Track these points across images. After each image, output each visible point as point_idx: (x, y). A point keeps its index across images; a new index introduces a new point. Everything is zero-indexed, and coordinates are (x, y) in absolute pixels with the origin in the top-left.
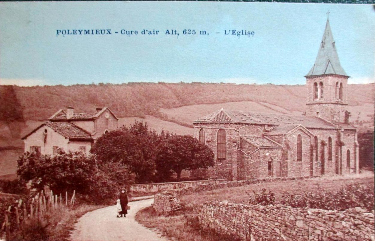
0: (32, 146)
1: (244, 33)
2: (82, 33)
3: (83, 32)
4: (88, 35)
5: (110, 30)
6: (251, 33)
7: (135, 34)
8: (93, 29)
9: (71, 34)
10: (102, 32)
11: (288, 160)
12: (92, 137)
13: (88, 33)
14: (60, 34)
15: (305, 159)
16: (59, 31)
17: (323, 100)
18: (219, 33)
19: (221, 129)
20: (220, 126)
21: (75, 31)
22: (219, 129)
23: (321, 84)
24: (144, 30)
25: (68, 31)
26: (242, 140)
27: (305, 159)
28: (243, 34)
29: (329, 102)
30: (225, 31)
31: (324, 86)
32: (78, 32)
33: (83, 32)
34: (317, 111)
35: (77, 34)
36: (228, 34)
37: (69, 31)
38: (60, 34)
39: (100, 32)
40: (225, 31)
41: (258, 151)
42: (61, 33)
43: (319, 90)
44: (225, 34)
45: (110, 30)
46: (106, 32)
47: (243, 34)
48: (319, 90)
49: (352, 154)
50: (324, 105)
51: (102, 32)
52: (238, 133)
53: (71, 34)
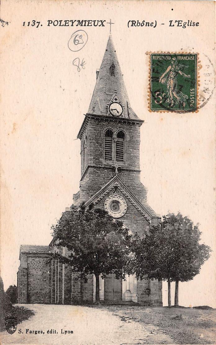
1: (189, 24)
3: (76, 23)
9: (63, 25)
14: (51, 25)
47: (188, 25)
53: (63, 25)
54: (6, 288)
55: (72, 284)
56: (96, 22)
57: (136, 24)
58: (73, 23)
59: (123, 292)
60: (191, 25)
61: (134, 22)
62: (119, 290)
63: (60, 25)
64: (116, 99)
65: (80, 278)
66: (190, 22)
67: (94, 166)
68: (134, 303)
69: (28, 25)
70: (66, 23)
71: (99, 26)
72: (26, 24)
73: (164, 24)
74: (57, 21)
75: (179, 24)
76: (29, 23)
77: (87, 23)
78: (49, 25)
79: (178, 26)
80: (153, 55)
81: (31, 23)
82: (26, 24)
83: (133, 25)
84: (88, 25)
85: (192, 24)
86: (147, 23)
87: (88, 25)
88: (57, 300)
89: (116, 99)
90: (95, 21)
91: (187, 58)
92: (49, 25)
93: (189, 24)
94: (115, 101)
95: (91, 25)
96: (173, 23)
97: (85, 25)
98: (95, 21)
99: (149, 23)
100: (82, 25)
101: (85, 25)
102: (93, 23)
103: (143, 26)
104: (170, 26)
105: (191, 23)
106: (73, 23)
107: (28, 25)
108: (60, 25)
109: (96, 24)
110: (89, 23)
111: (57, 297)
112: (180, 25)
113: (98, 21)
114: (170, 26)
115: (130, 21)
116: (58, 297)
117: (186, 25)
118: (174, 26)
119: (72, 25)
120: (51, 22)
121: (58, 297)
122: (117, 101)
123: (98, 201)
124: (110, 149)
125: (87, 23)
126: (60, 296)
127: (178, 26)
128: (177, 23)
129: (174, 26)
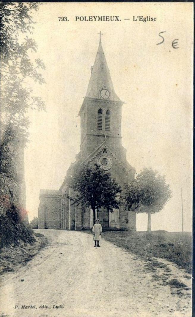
0: (40, 85)
2: (96, 20)
3: (97, 19)
4: (100, 21)
5: (118, 17)
6: (153, 19)
8: (134, 16)
9: (88, 20)
10: (111, 19)
12: (178, 296)
13: (101, 20)
14: (78, 20)
16: (77, 18)
24: (147, 17)
25: (85, 17)
30: (134, 17)
32: (93, 19)
33: (88, 18)
35: (92, 20)
36: (136, 20)
37: (86, 18)
38: (78, 20)
39: (110, 18)
40: (134, 17)
42: (79, 19)
44: (134, 20)
45: (118, 17)
46: (115, 18)
47: (147, 20)
49: (191, 303)
51: (111, 19)
53: (88, 20)
55: (76, 216)
59: (110, 222)
60: (149, 20)
62: (107, 220)
64: (105, 87)
66: (149, 17)
67: (90, 134)
68: (118, 229)
70: (90, 18)
73: (129, 19)
74: (112, 20)
85: (151, 19)
87: (106, 20)
88: (65, 227)
89: (105, 87)
94: (104, 88)
105: (150, 18)
109: (112, 19)
111: (65, 225)
116: (66, 225)
121: (66, 225)
122: (106, 88)
123: (93, 158)
124: (101, 121)
126: (67, 224)
129: (136, 20)
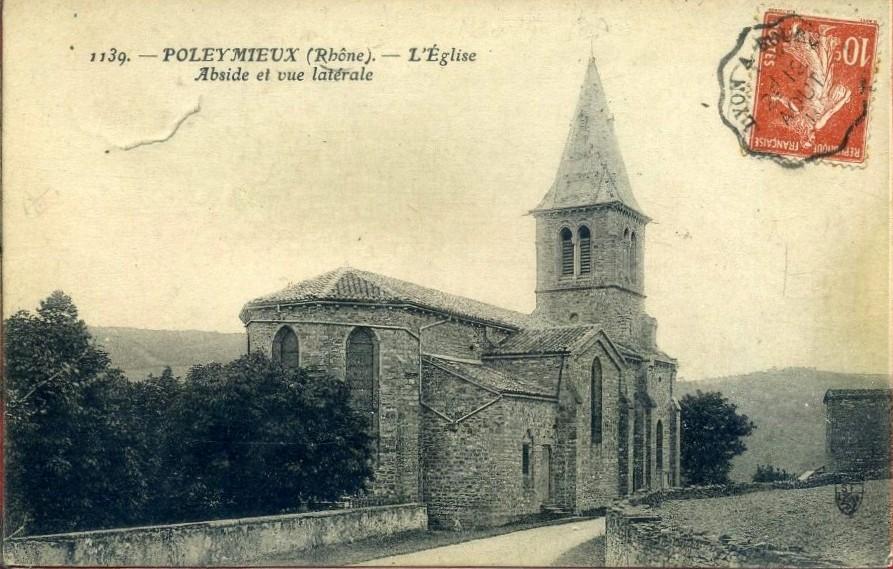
1: (455, 57)
2: (224, 58)
3: (230, 55)
7: (272, 61)
9: (199, 60)
11: (577, 440)
14: (172, 58)
15: (609, 437)
17: (587, 279)
18: (470, 57)
19: (360, 330)
20: (356, 318)
21: (210, 52)
22: (352, 329)
23: (585, 232)
26: (426, 362)
27: (609, 437)
28: (452, 59)
29: (608, 284)
31: (594, 238)
34: (572, 312)
41: (496, 406)
43: (577, 251)
47: (452, 59)
48: (577, 251)
50: (594, 292)
52: (415, 343)
53: (199, 60)
54: (7, 316)
56: (277, 52)
57: (327, 57)
58: (222, 54)
60: (458, 60)
61: (322, 52)
63: (192, 60)
65: (408, 493)
66: (457, 51)
69: (102, 60)
70: (206, 55)
71: (285, 60)
72: (98, 57)
75: (431, 55)
76: (103, 55)
77: (256, 56)
78: (166, 59)
79: (429, 60)
80: (858, 159)
81: (109, 55)
82: (98, 57)
83: (321, 58)
84: (259, 60)
85: (461, 57)
86: (349, 54)
87: (259, 60)
90: (275, 50)
91: (773, 144)
92: (166, 59)
93: (455, 57)
95: (266, 60)
96: (418, 54)
97: (251, 60)
98: (275, 50)
99: (354, 54)
100: (243, 60)
101: (251, 60)
102: (270, 54)
103: (184, 62)
104: (412, 59)
106: (222, 54)
107: (102, 60)
108: (192, 60)
109: (277, 57)
110: (260, 55)
112: (433, 58)
113: (282, 49)
114: (412, 59)
115: (311, 49)
117: (448, 59)
118: (419, 60)
119: (221, 59)
120: (171, 52)
125: (256, 56)
127: (429, 60)
128: (428, 53)
129: (419, 60)
